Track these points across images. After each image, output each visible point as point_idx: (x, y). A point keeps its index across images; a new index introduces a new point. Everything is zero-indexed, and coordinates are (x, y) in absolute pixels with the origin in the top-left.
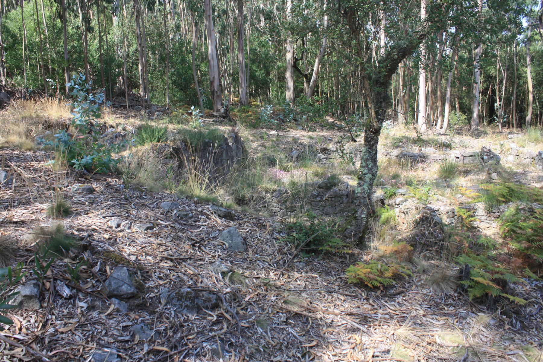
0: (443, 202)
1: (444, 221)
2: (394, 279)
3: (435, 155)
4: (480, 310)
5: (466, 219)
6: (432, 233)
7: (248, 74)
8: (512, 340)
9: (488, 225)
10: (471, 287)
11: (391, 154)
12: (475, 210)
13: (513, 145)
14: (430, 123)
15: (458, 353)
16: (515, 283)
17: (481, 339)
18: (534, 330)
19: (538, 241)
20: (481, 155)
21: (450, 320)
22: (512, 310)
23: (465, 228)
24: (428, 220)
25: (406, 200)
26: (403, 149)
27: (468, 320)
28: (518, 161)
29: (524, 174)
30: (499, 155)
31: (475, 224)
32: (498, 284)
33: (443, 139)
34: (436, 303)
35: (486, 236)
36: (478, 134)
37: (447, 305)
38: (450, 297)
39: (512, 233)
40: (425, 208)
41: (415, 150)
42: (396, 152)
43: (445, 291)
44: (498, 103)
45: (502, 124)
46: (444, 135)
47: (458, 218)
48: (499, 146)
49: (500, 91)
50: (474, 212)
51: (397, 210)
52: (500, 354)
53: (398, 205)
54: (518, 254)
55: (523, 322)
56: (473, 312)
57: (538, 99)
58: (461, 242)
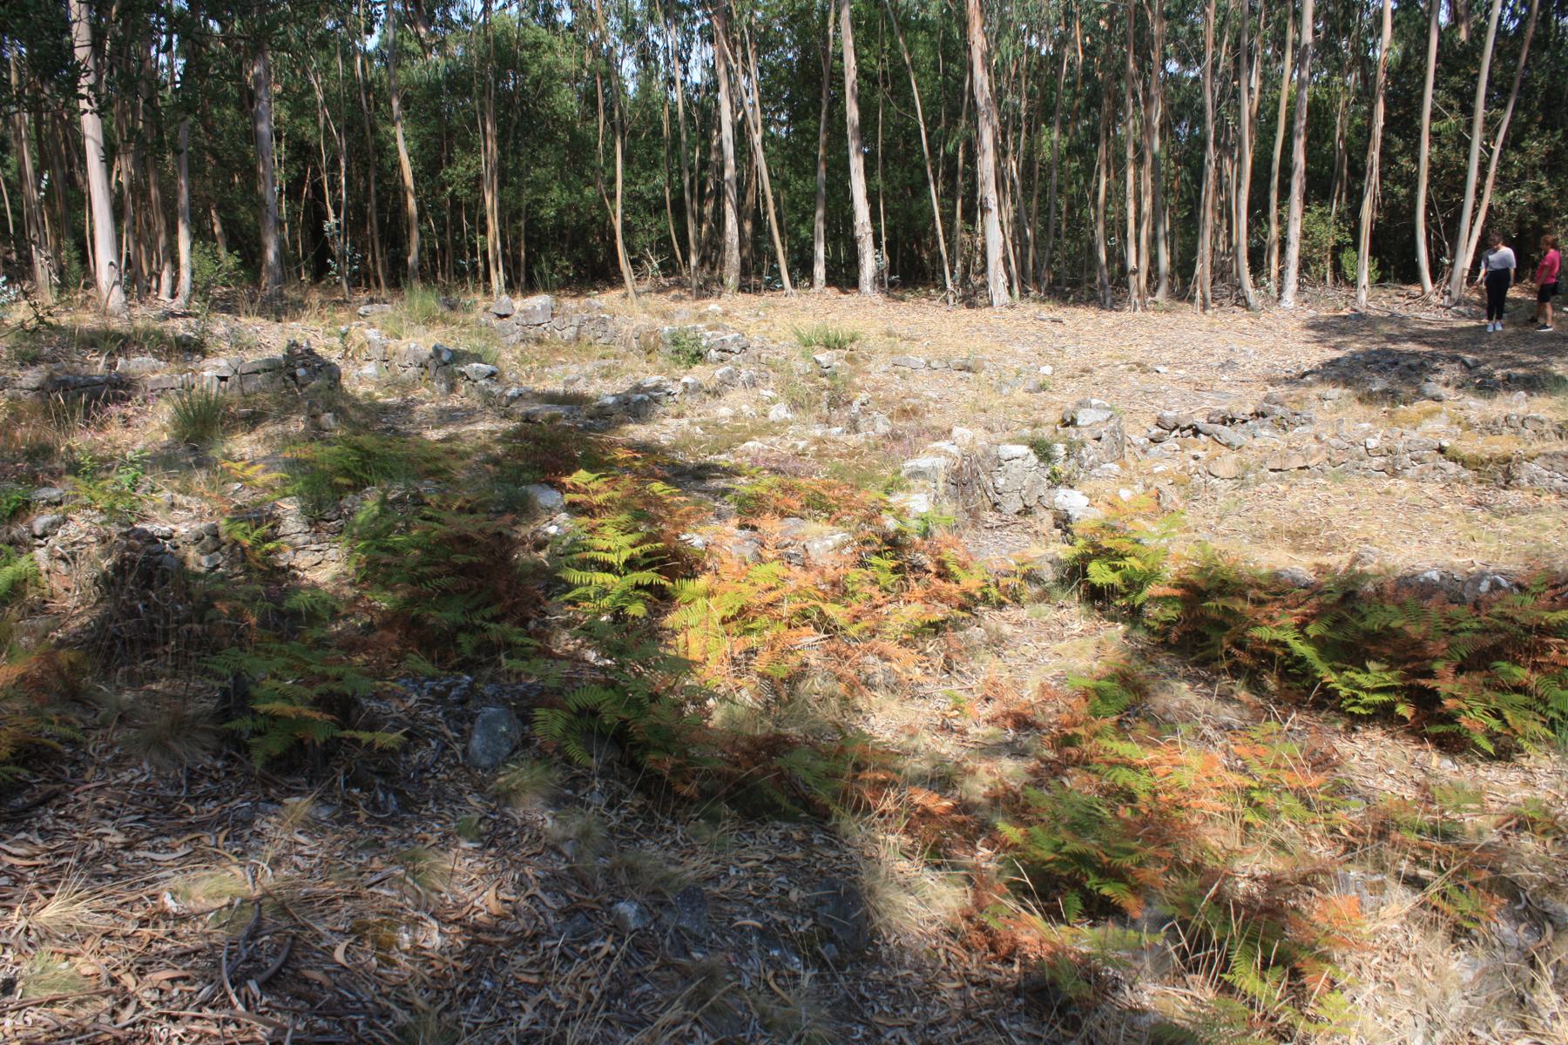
0: (190, 510)
1: (191, 565)
2: (23, 763)
3: (157, 376)
4: (288, 790)
5: (253, 548)
6: (156, 604)
7: (1274, 230)
8: (377, 845)
9: (318, 557)
10: (260, 733)
11: (18, 384)
12: (276, 522)
13: (372, 334)
14: (136, 281)
15: (232, 922)
16: (378, 697)
17: (297, 866)
18: (431, 805)
19: (435, 577)
20: (288, 365)
21: (206, 840)
22: (373, 768)
23: (255, 575)
24: (142, 568)
25: (65, 520)
26: (53, 366)
27: (259, 824)
28: (387, 375)
29: (404, 408)
30: (340, 363)
31: (283, 560)
32: (329, 709)
33: (179, 327)
34: (160, 800)
35: (314, 586)
36: (278, 309)
37: (197, 799)
38: (202, 776)
39: (374, 572)
40: (126, 535)
41: (97, 364)
42: (31, 377)
43: (187, 761)
44: (332, 220)
45: (348, 280)
46: (184, 315)
47: (232, 549)
48: (337, 340)
49: (334, 187)
50: (273, 527)
51: (40, 553)
52: (348, 889)
53: (41, 537)
54: (390, 621)
55: (403, 792)
56: (271, 801)
57: (431, 210)
58: (237, 614)
